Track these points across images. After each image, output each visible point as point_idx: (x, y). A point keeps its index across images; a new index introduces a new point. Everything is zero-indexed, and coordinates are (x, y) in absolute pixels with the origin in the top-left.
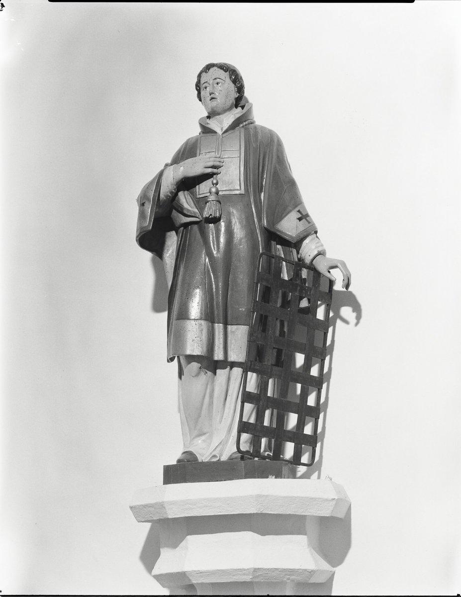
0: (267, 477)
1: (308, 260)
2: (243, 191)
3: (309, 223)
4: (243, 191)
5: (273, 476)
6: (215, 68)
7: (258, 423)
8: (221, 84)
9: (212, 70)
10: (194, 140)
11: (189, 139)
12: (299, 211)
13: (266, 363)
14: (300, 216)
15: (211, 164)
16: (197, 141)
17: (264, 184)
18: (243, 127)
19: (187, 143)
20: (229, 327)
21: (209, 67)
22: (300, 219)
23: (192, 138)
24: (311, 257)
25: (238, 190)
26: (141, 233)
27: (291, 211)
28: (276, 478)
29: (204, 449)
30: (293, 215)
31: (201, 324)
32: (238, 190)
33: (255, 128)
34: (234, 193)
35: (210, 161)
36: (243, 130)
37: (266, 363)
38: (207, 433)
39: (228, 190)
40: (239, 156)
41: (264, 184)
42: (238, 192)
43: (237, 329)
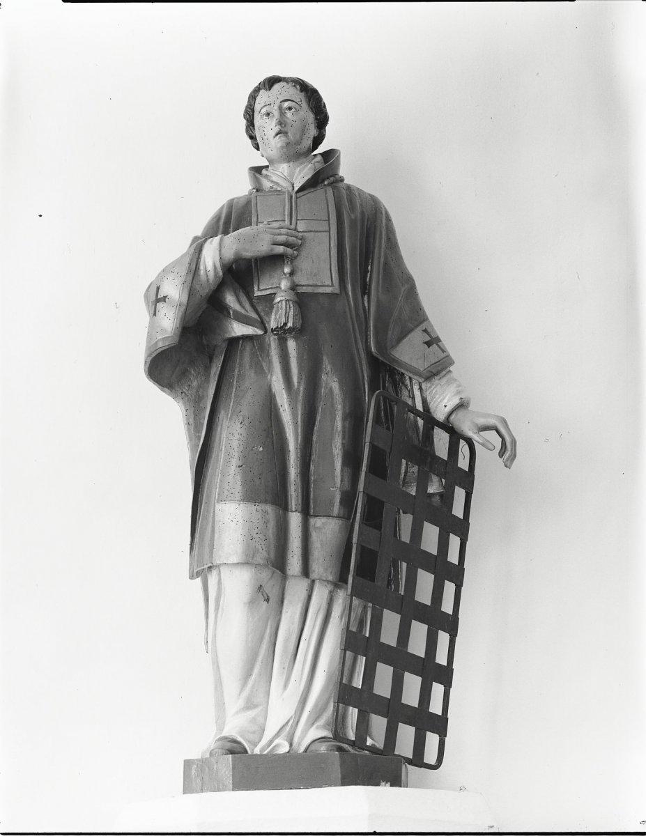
0: (378, 785)
1: (440, 415)
2: (336, 289)
3: (443, 351)
4: (336, 289)
5: (387, 783)
6: (282, 84)
7: (364, 687)
8: (293, 110)
9: (277, 87)
10: (242, 202)
11: (233, 199)
12: (425, 331)
13: (379, 584)
14: (428, 338)
15: (282, 238)
16: (248, 202)
17: (368, 280)
18: (329, 185)
19: (231, 204)
20: (312, 521)
21: (271, 82)
22: (429, 344)
23: (238, 198)
24: (448, 409)
25: (328, 286)
26: (149, 356)
27: (412, 330)
28: (391, 786)
29: (254, 732)
30: (417, 337)
31: (266, 512)
32: (328, 286)
33: (349, 188)
34: (321, 290)
35: (281, 234)
36: (330, 191)
37: (379, 584)
38: (260, 705)
39: (311, 286)
40: (327, 229)
41: (368, 280)
42: (329, 290)
43: (324, 524)
